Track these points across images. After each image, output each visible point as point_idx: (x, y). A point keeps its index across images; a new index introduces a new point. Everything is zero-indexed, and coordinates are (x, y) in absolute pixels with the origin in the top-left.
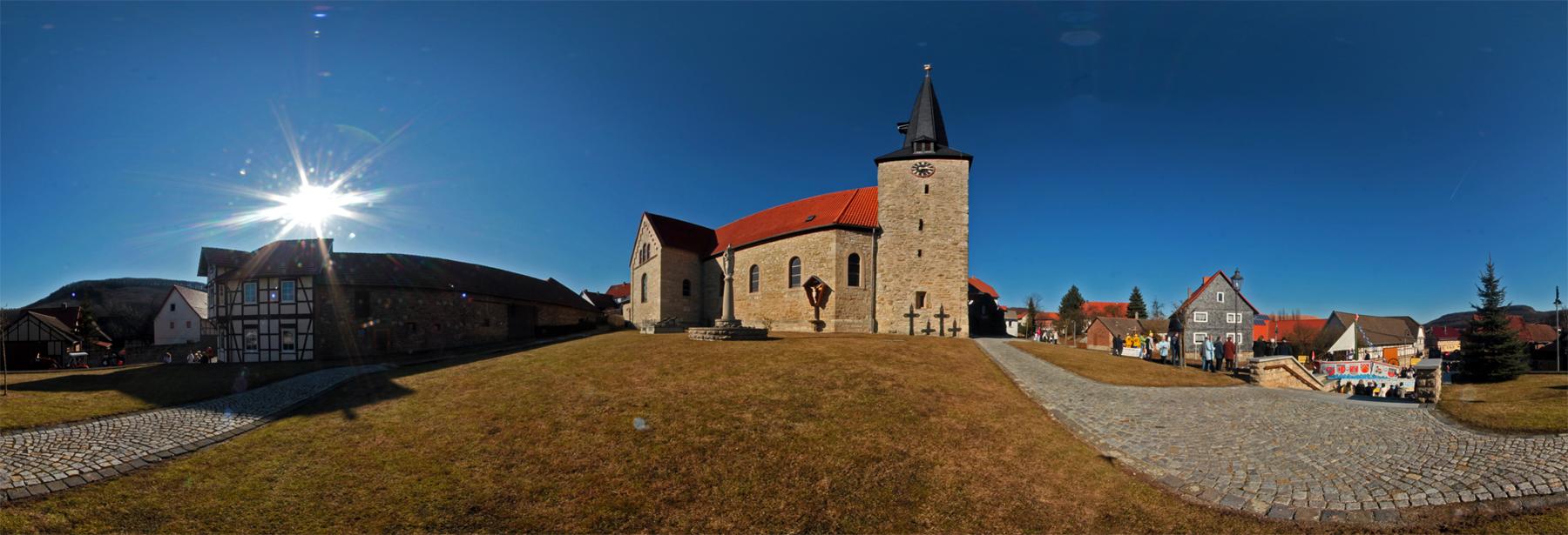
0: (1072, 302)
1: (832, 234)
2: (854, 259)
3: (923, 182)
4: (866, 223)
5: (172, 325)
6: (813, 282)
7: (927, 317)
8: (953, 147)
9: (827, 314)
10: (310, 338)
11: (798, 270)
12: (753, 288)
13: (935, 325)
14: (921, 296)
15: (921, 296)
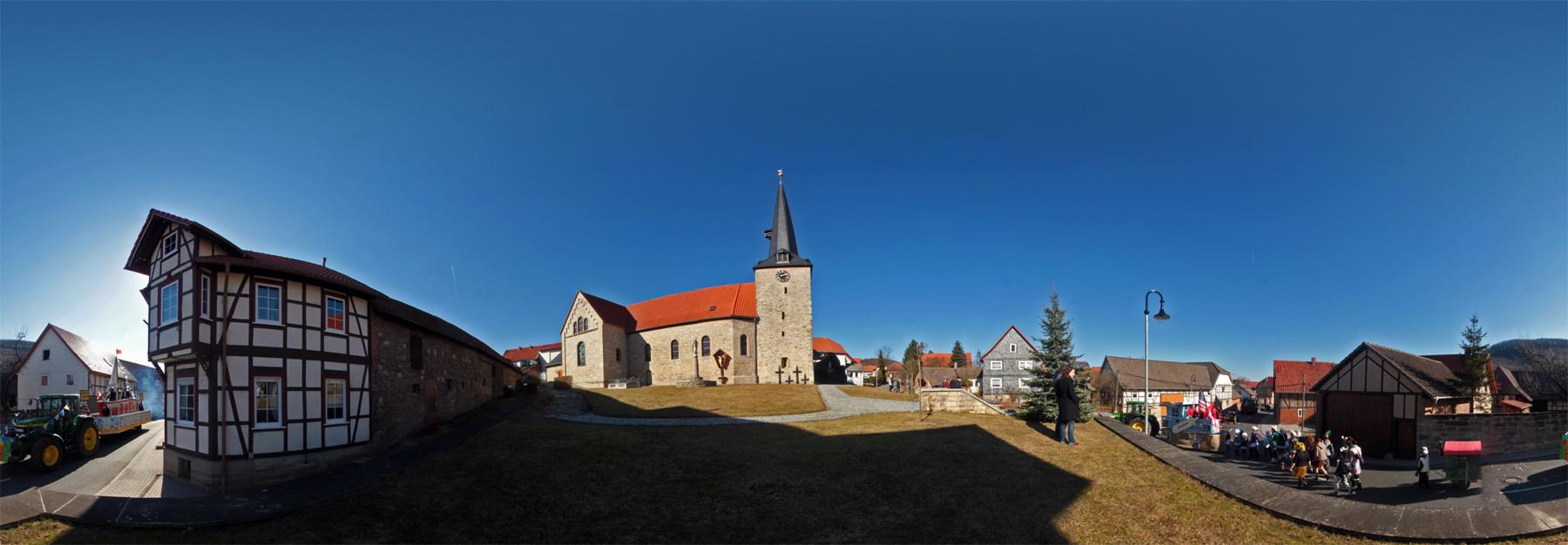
0: (913, 351)
1: (730, 322)
2: (743, 338)
3: (784, 285)
4: (750, 315)
5: (44, 381)
6: (720, 353)
7: (789, 372)
8: (802, 254)
9: (729, 373)
10: (366, 395)
13: (794, 377)
14: (784, 360)
15: (784, 360)
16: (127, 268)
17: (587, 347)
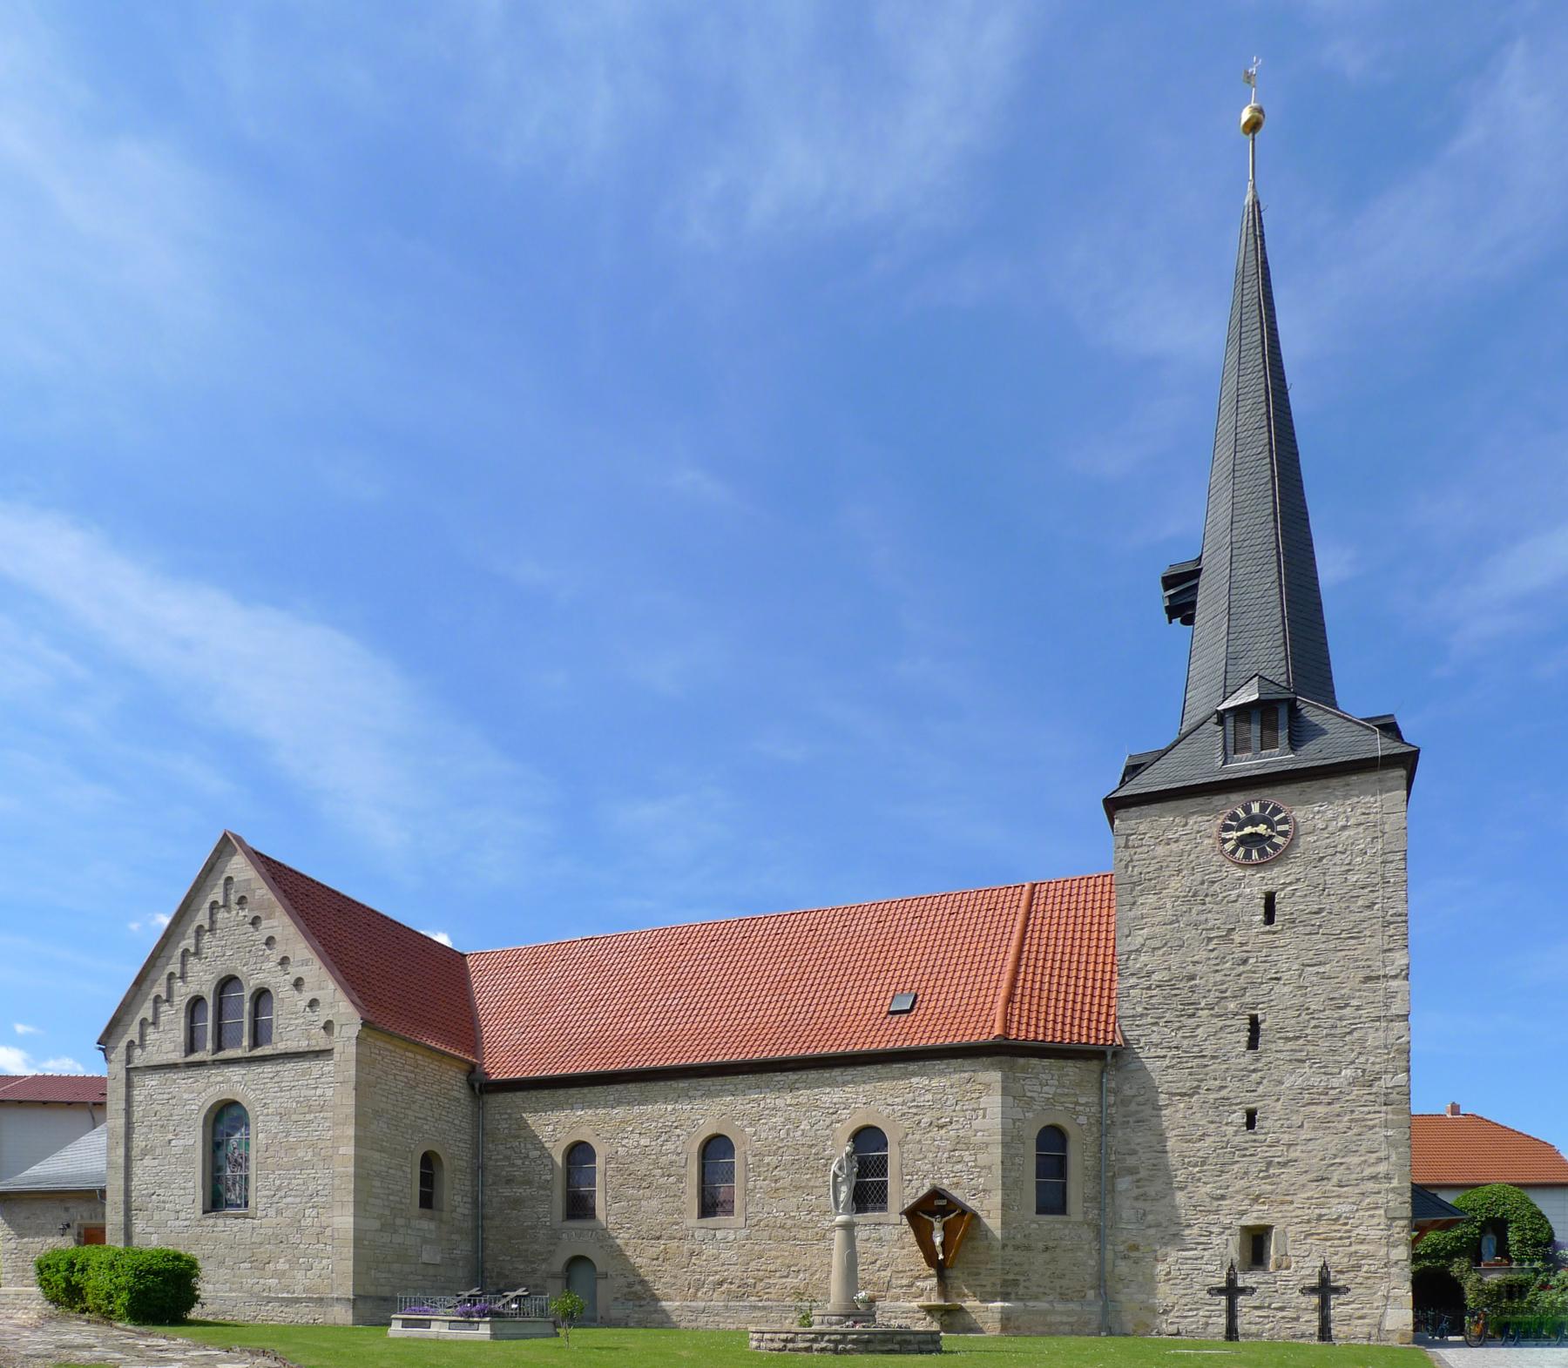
2: (1053, 1142)
3: (1255, 885)
11: (881, 1166)
12: (429, 1162)
14: (1256, 1243)
15: (1256, 1243)
16: (1271, 1227)
17: (261, 1135)
